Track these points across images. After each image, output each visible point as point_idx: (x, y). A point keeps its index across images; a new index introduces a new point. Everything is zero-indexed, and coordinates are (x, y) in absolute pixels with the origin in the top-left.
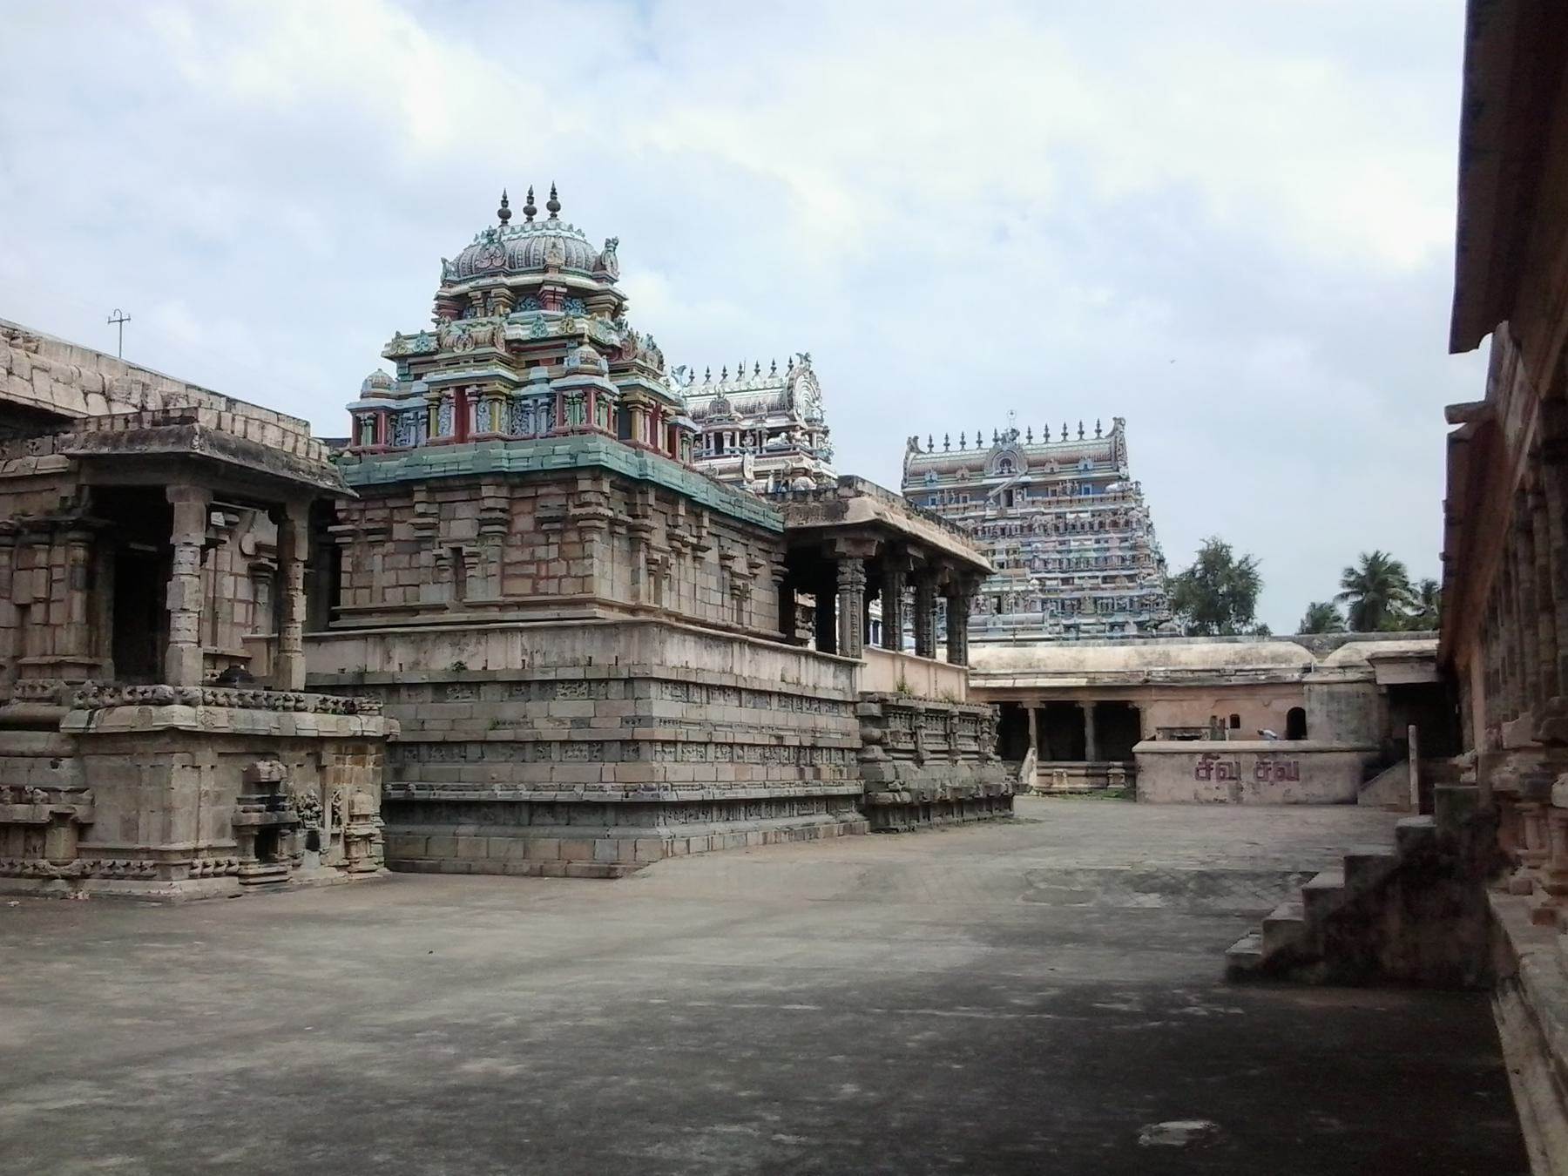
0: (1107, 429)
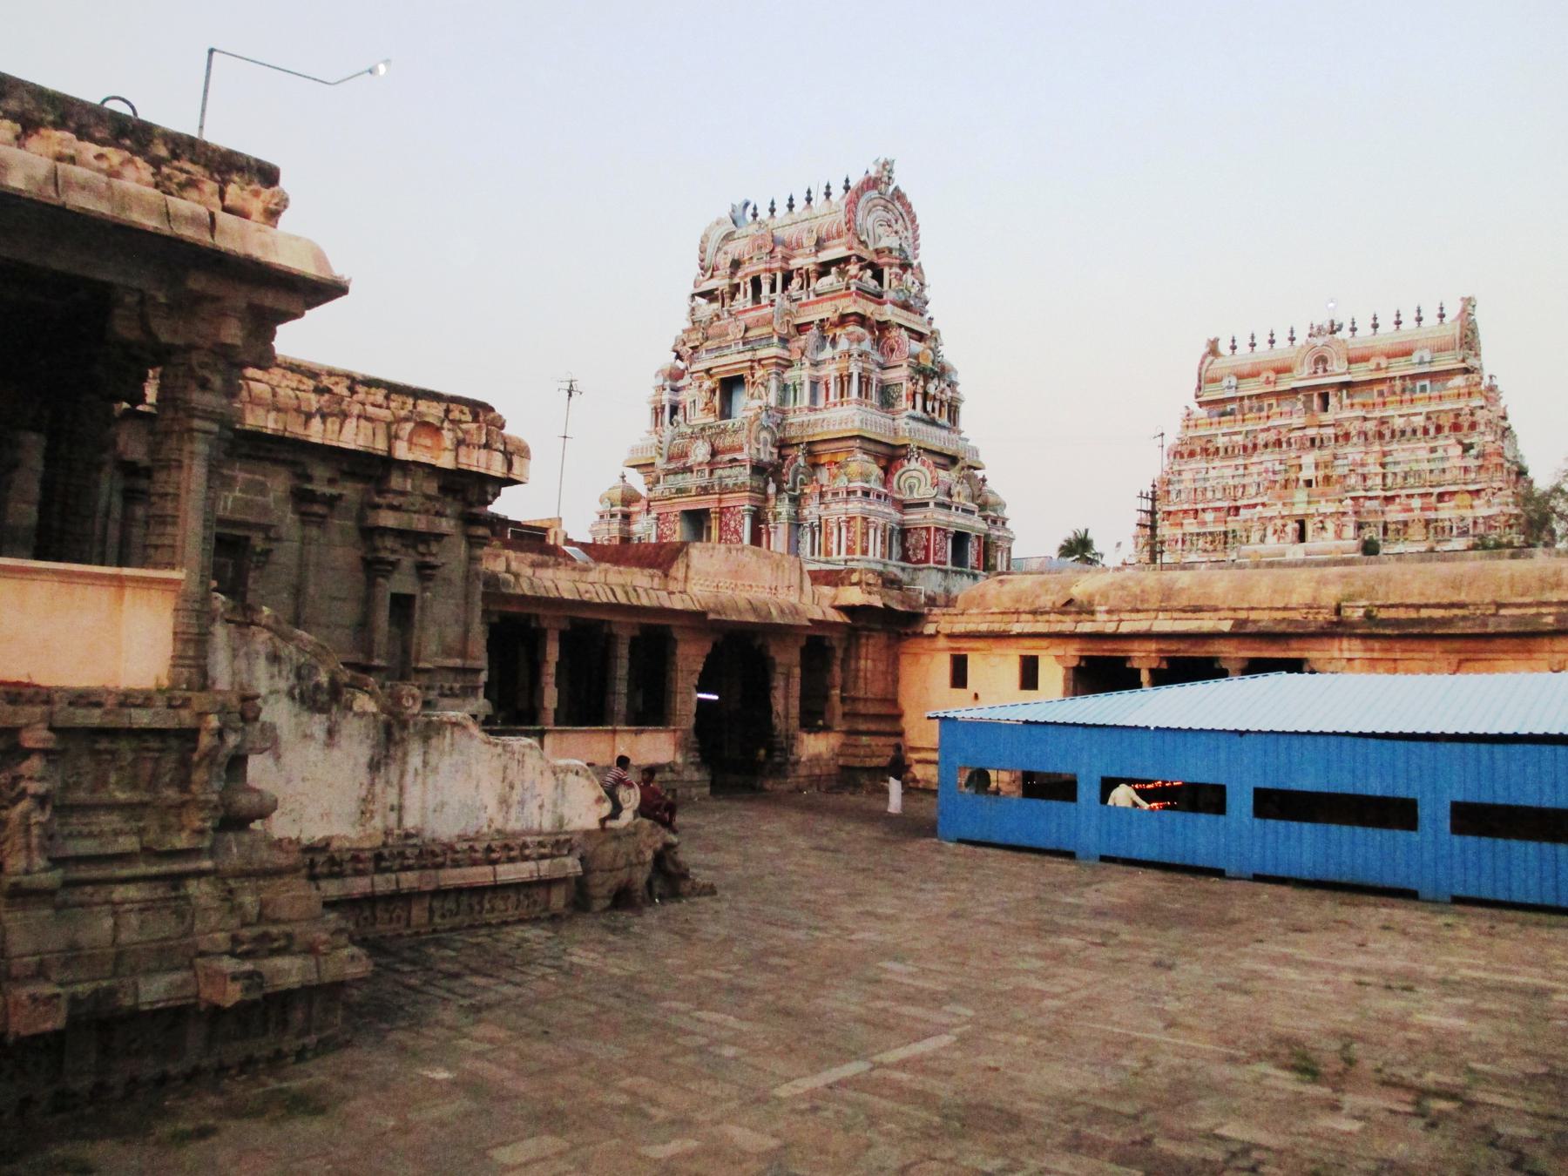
0: (1452, 312)
